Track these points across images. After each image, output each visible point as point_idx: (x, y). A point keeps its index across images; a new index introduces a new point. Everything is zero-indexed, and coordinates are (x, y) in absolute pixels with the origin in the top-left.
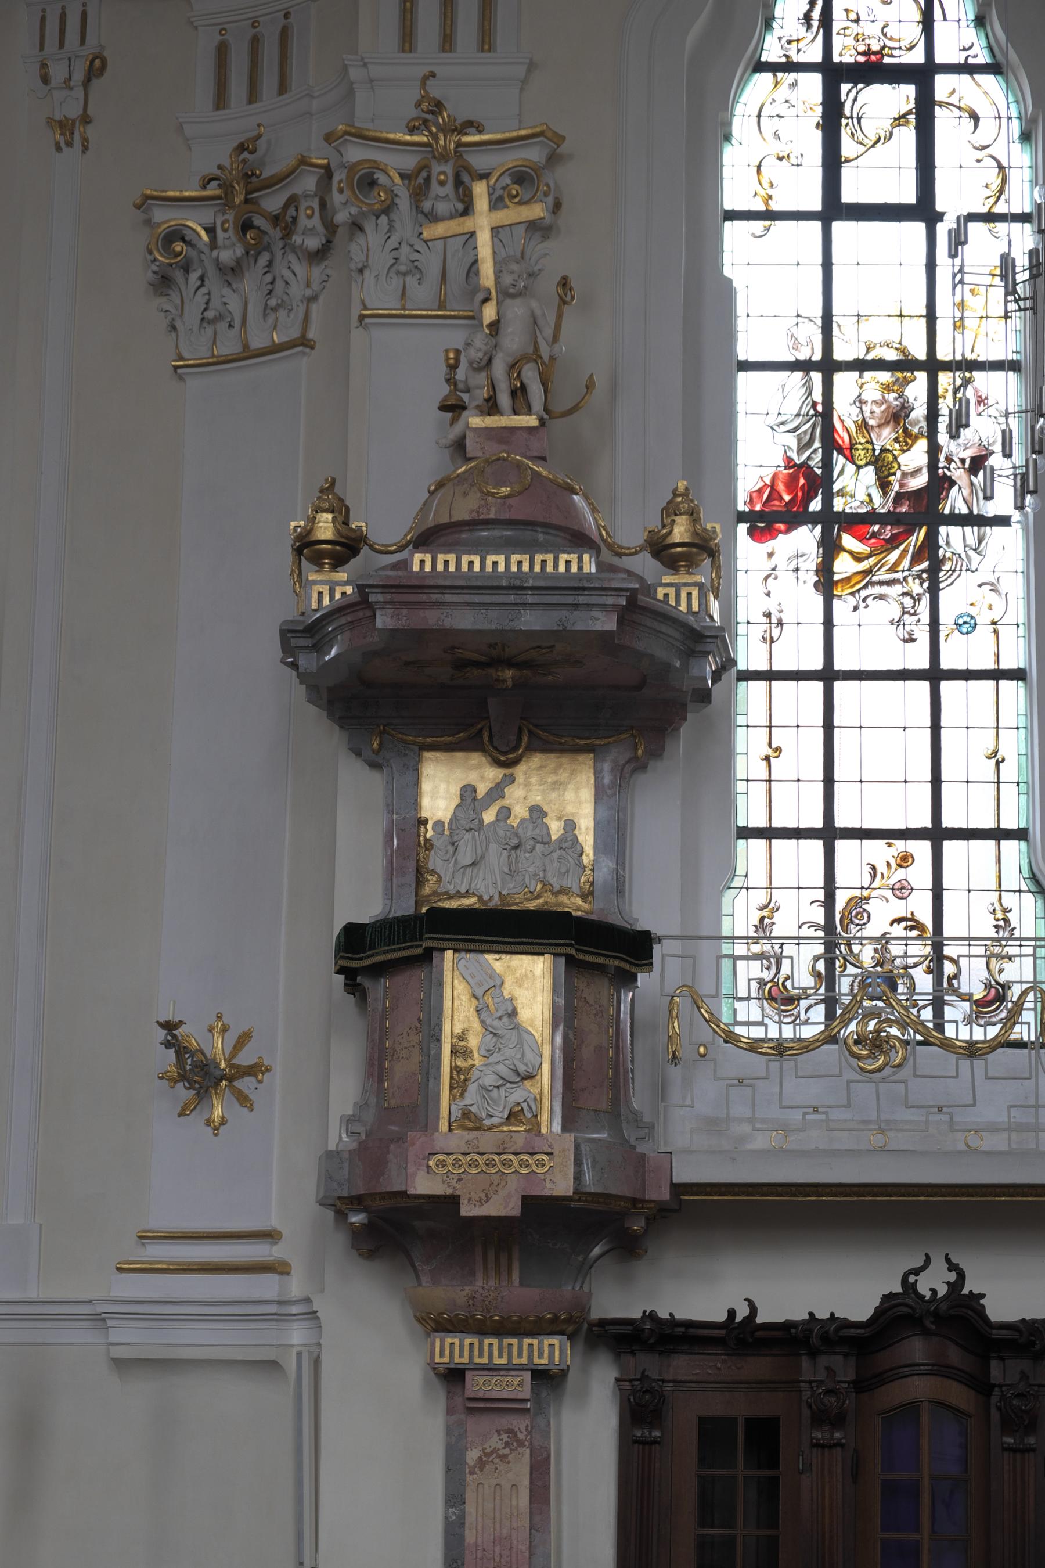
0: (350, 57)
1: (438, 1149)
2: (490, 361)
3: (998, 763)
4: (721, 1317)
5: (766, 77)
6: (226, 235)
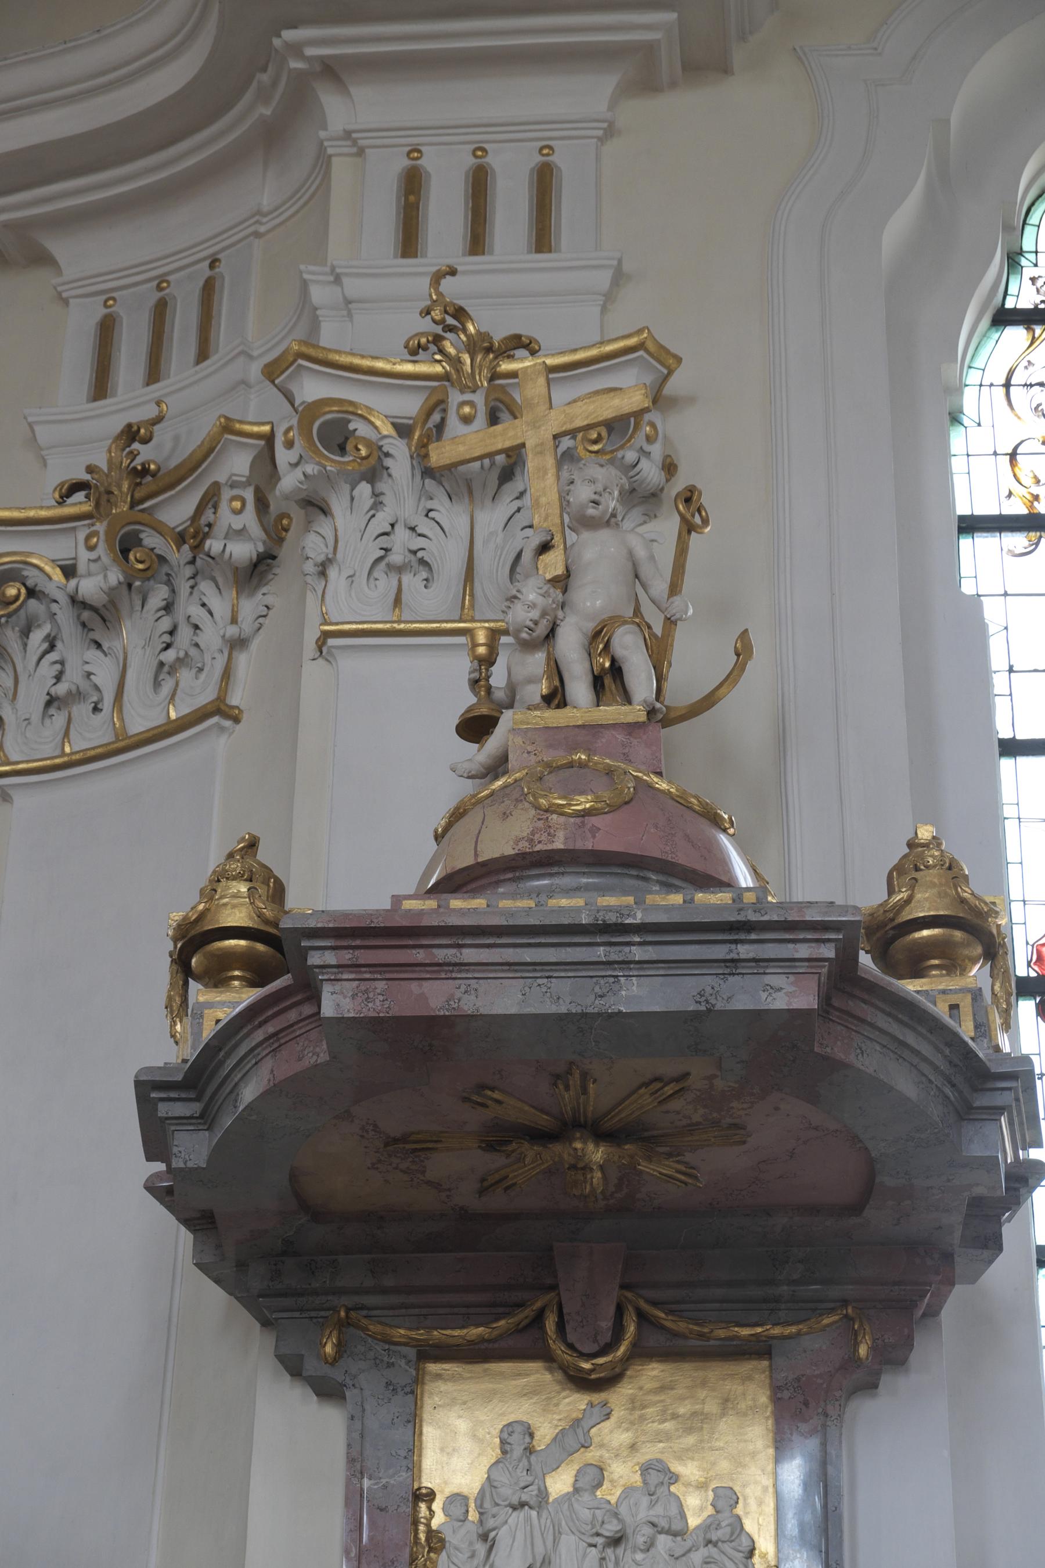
0: (312, 268)
2: (551, 634)
5: (1015, 335)
6: (93, 555)
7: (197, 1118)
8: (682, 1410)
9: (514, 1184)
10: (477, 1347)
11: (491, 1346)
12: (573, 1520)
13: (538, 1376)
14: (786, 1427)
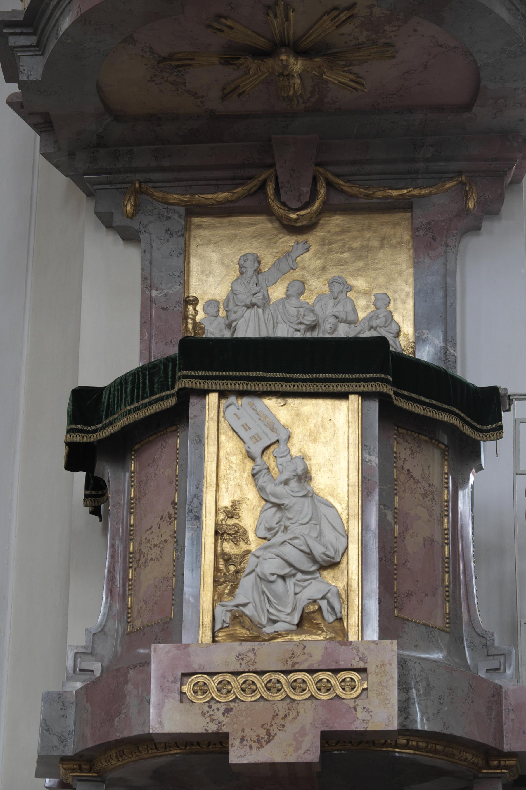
7: (34, 47)
8: (355, 245)
9: (245, 91)
10: (223, 206)
11: (232, 205)
12: (285, 315)
13: (264, 225)
14: (421, 254)
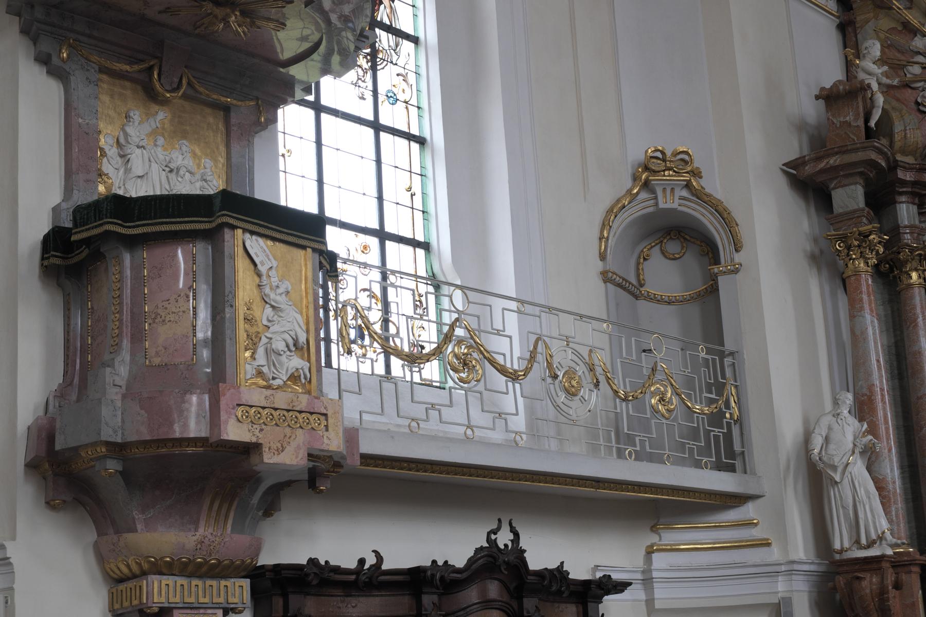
1: (244, 402)
3: (412, 195)
4: (352, 565)
